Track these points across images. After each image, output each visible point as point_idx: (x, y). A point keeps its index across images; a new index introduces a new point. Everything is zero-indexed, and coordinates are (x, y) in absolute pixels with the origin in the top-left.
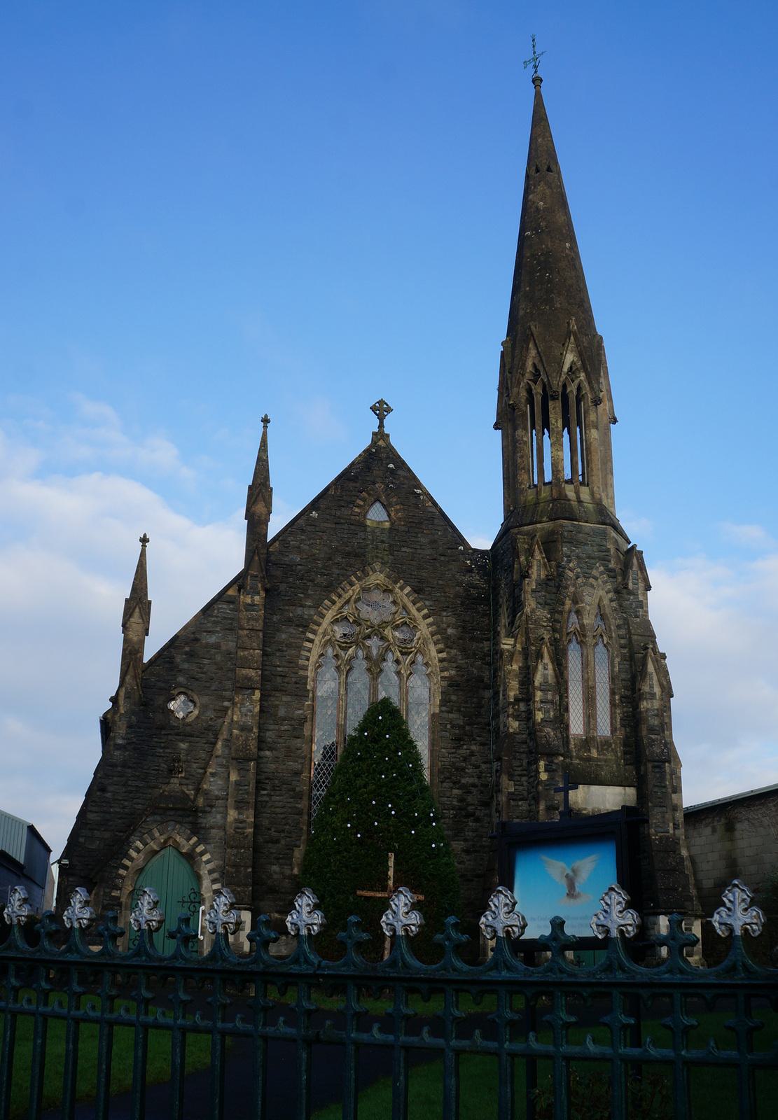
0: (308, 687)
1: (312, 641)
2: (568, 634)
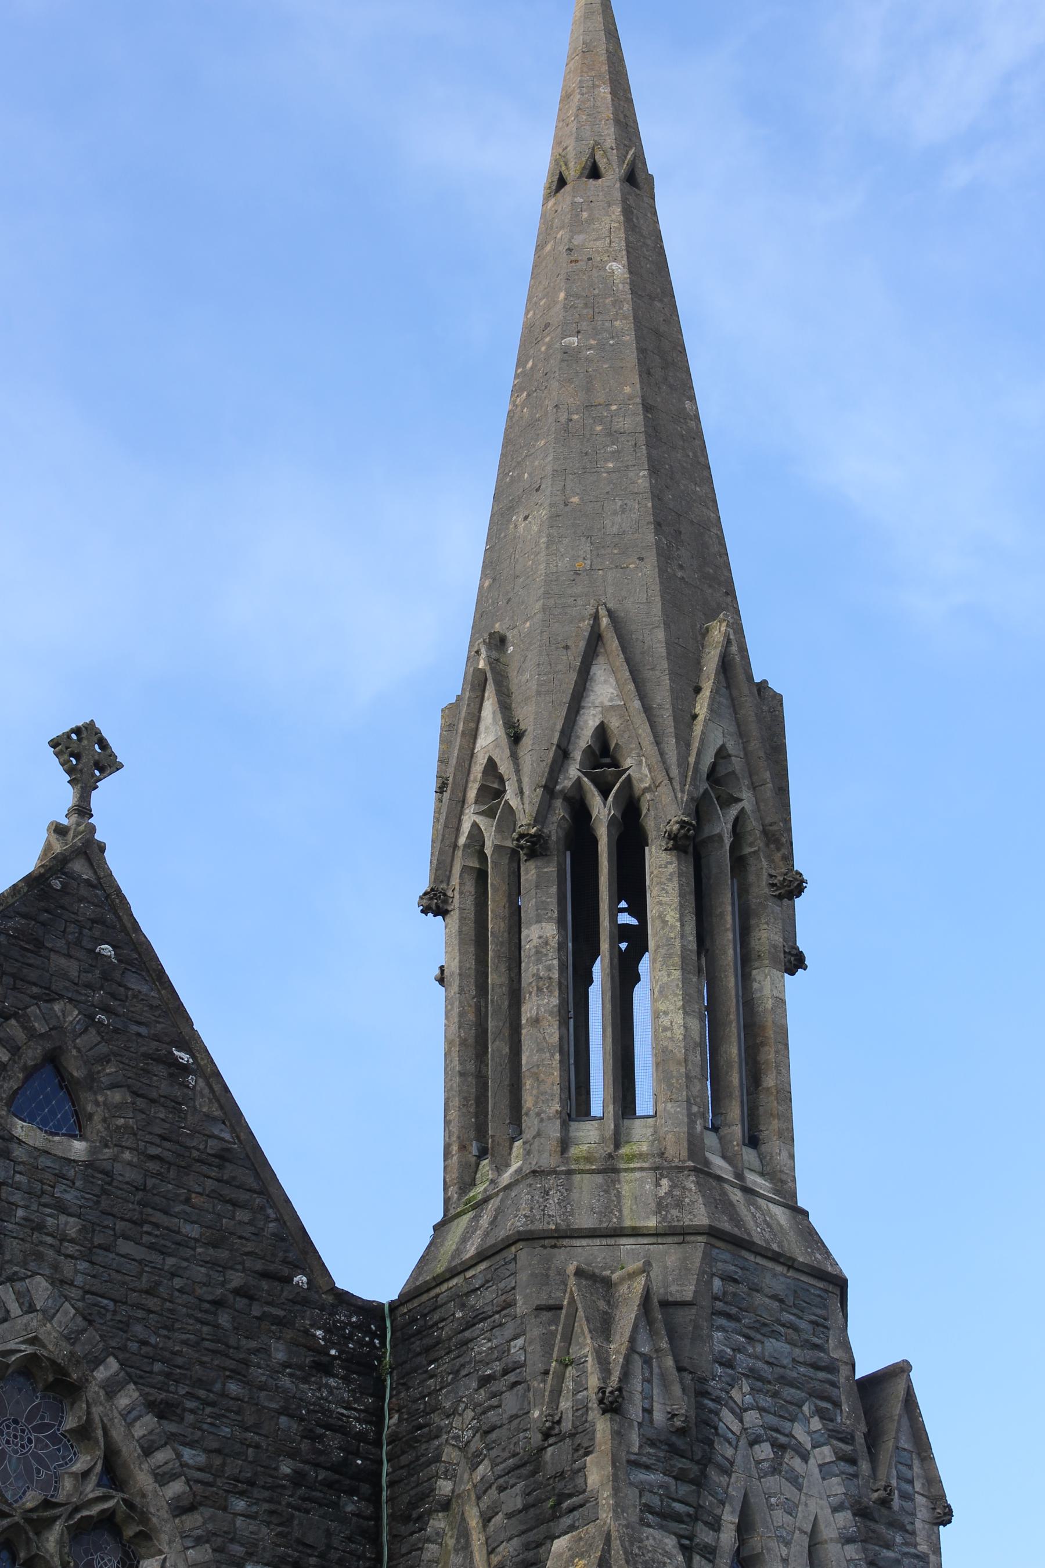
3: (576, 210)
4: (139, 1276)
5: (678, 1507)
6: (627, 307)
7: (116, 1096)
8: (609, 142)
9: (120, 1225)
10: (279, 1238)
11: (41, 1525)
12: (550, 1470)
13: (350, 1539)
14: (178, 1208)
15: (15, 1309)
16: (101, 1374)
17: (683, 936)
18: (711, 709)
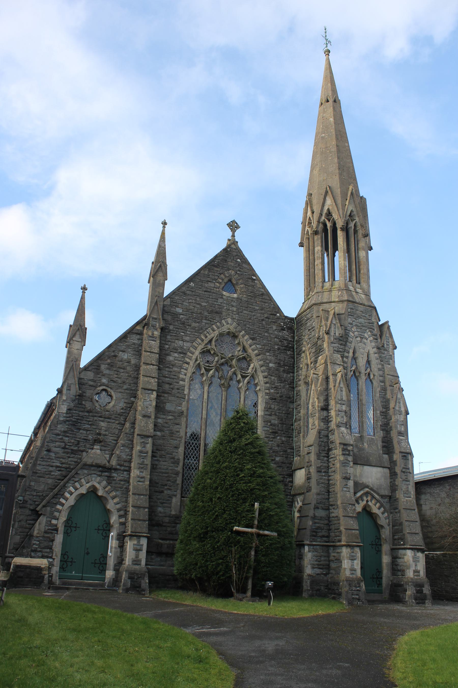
0: (185, 393)
1: (188, 363)
2: (351, 371)
3: (324, 109)
4: (248, 317)
5: (341, 350)
6: (333, 127)
7: (242, 286)
8: (330, 94)
9: (244, 308)
10: (274, 308)
11: (232, 360)
12: (318, 345)
13: (289, 358)
14: (254, 304)
15: (225, 324)
16: (241, 334)
18: (349, 203)
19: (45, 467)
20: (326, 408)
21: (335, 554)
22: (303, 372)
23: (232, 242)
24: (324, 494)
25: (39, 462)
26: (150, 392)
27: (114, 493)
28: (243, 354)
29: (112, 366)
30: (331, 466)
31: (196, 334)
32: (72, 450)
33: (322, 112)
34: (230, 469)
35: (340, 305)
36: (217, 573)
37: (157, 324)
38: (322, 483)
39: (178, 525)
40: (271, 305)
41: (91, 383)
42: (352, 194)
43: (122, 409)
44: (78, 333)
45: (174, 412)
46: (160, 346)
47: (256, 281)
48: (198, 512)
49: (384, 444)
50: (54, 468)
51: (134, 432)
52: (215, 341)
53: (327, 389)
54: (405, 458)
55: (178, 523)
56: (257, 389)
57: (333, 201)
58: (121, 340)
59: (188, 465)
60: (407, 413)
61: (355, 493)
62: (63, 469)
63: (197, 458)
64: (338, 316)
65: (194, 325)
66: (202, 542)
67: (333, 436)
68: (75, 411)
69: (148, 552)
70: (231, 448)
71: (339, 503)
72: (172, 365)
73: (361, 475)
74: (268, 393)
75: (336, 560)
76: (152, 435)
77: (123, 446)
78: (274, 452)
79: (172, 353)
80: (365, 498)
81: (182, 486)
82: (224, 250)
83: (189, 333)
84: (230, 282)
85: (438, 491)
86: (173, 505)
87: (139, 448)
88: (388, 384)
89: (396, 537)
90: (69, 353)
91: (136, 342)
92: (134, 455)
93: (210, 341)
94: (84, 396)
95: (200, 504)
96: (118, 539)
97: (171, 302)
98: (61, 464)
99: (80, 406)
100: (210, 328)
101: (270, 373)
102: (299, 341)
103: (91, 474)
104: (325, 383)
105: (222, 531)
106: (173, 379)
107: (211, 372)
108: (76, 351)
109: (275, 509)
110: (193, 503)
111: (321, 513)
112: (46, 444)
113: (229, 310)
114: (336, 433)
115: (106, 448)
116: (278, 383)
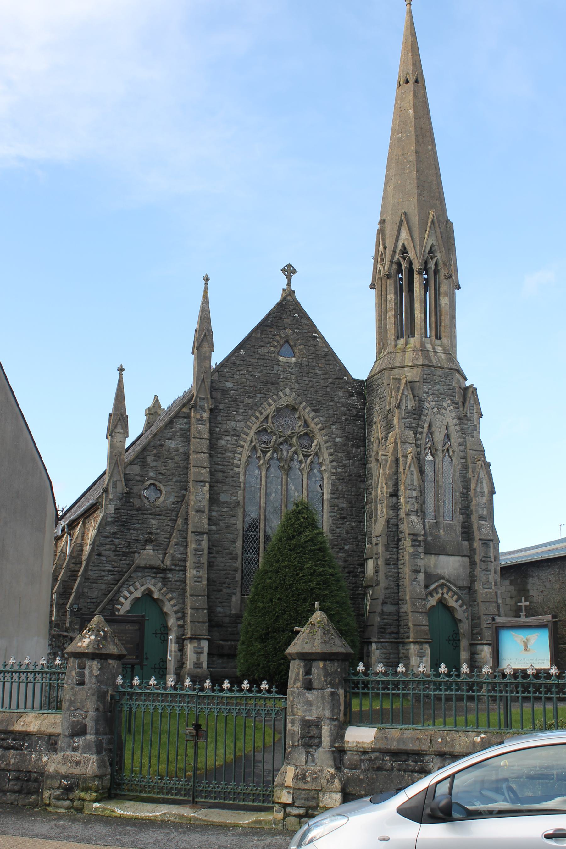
0: (241, 480)
1: (242, 447)
2: (425, 449)
5: (414, 425)
6: (413, 123)
7: (301, 347)
8: (411, 72)
9: (304, 374)
11: (292, 437)
12: (389, 419)
14: (316, 368)
15: (282, 396)
16: (302, 406)
17: (420, 295)
19: (96, 572)
20: (395, 494)
21: (404, 651)
22: (374, 447)
23: (287, 292)
24: (393, 588)
25: (90, 568)
26: (202, 484)
27: (170, 595)
28: (305, 430)
29: (159, 457)
30: (401, 558)
31: (250, 411)
32: (123, 552)
33: (400, 98)
34: (289, 568)
35: (415, 370)
36: (279, 673)
37: (206, 405)
38: (391, 576)
39: (239, 625)
40: (337, 366)
41: (138, 478)
42: (433, 222)
43: (173, 503)
44: (119, 423)
45: (230, 503)
46: (210, 430)
47: (318, 339)
48: (259, 613)
49: (464, 530)
50: (107, 572)
51: (187, 529)
52: (272, 418)
53: (397, 473)
54: (485, 546)
55: (238, 623)
56: (321, 470)
57: (409, 234)
58: (166, 426)
59: (247, 560)
60: (492, 492)
61: (427, 587)
62: (115, 573)
63: (256, 551)
64: (411, 384)
65: (247, 400)
66: (264, 642)
67: (403, 525)
68: (124, 510)
69: (208, 654)
70: (290, 546)
71: (408, 597)
72: (225, 451)
73: (435, 566)
74: (334, 473)
75: (405, 657)
76: (207, 531)
77: (176, 545)
78: (342, 540)
79: (223, 436)
80: (440, 591)
81: (242, 583)
82: (278, 304)
83: (242, 411)
84: (287, 345)
85: (546, 574)
86: (233, 604)
87: (194, 546)
88: (469, 461)
89: (474, 632)
90: (112, 447)
91: (183, 427)
92: (189, 554)
93: (267, 418)
94: (132, 493)
95: (260, 604)
96: (177, 642)
97: (220, 376)
98: (113, 567)
99: (128, 504)
100: (265, 403)
101: (337, 448)
102: (370, 409)
103: (145, 577)
104: (394, 466)
105: (283, 631)
106: (227, 466)
107: (269, 454)
108: (119, 444)
109: (335, 608)
110: (253, 604)
111: (389, 608)
112: (96, 548)
113: (286, 378)
114: (405, 522)
115: (158, 548)
116: (346, 460)
